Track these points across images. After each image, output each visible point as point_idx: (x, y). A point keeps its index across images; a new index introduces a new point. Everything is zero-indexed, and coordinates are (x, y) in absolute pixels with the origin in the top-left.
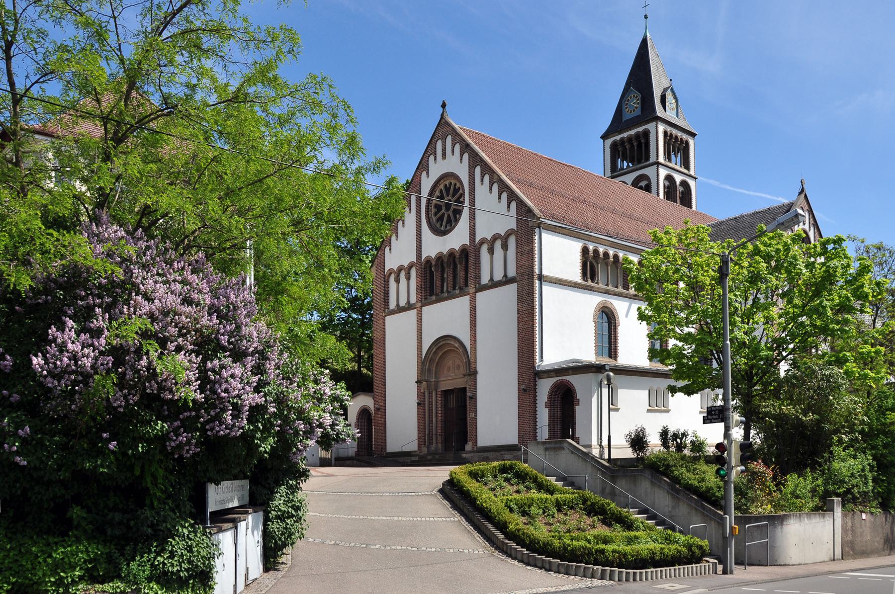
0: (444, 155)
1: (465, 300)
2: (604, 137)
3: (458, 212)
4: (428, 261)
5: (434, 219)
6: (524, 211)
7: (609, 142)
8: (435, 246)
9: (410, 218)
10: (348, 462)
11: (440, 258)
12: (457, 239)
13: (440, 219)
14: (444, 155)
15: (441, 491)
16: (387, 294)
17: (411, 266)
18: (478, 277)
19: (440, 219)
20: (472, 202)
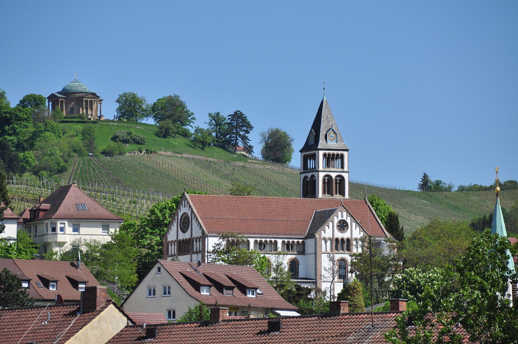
0: (185, 206)
1: (190, 255)
2: (301, 151)
3: (188, 226)
4: (180, 240)
5: (182, 226)
6: (203, 232)
7: (303, 154)
8: (182, 236)
9: (175, 224)
10: (313, 137)
11: (183, 240)
12: (187, 236)
13: (184, 227)
14: (185, 206)
15: (252, 128)
16: (168, 249)
17: (175, 241)
18: (168, 252)
19: (184, 227)
20: (192, 225)
